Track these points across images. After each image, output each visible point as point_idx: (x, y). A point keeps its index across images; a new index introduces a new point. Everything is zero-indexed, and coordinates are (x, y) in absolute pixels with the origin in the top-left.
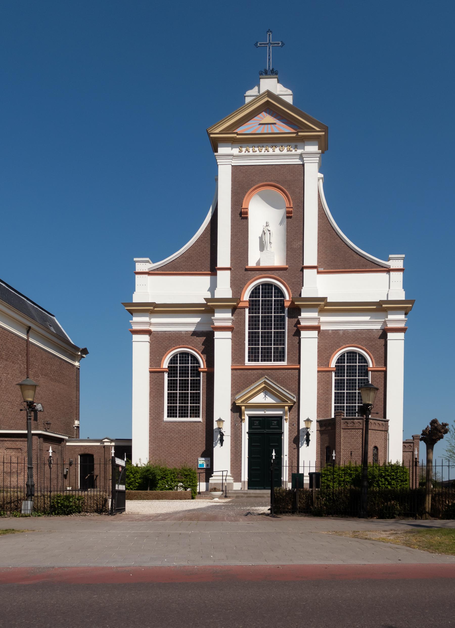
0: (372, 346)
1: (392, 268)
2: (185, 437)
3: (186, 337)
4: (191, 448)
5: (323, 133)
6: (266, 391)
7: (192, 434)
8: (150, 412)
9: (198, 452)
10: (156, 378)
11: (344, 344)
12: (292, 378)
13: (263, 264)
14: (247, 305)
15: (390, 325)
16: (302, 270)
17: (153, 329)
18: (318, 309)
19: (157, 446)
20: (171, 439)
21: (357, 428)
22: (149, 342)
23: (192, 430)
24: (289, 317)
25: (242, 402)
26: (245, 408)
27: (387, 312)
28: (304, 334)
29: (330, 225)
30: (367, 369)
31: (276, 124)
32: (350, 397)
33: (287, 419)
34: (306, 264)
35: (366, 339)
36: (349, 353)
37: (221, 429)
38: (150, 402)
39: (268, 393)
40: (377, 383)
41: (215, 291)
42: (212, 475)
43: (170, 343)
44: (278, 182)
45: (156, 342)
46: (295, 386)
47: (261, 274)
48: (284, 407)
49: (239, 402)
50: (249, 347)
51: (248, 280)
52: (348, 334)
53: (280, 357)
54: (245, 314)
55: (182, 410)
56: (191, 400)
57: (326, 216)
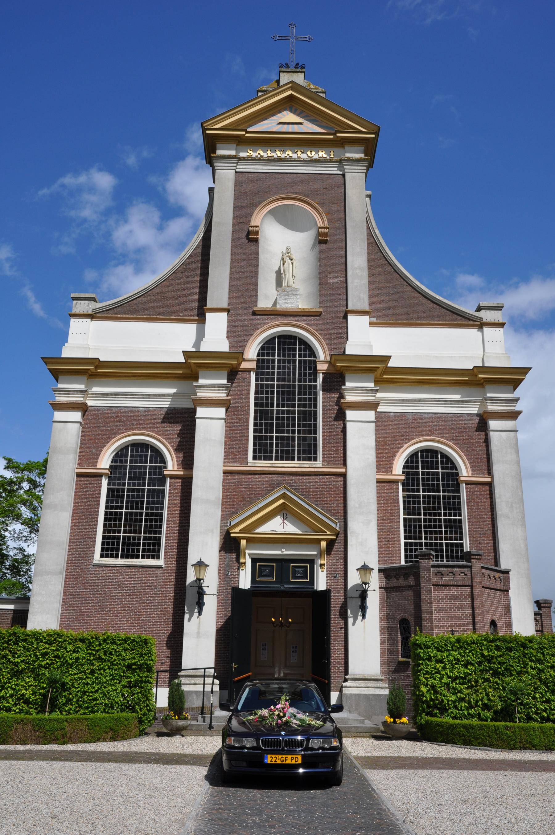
0: (463, 441)
1: (484, 321)
2: (130, 595)
3: (145, 417)
4: (139, 618)
5: (373, 136)
6: (284, 512)
7: (144, 590)
8: (69, 546)
9: (153, 625)
10: (87, 486)
11: (416, 435)
12: (331, 489)
13: (282, 306)
14: (253, 365)
15: (491, 407)
16: (345, 318)
17: (90, 402)
18: (372, 376)
19: (77, 612)
20: (104, 598)
21: (460, 583)
22: (80, 423)
23: (145, 583)
24: (324, 390)
25: (241, 531)
26: (247, 542)
27: (483, 387)
28: (350, 415)
29: (383, 257)
30: (457, 480)
31: (302, 124)
32: (430, 527)
33: (324, 565)
34: (351, 307)
35: (452, 429)
36: (425, 451)
37: (202, 581)
38: (72, 528)
39: (289, 516)
40: (478, 503)
41: (202, 342)
42: (179, 674)
43: (117, 427)
44: (305, 195)
45: (94, 424)
46: (337, 504)
47: (278, 320)
48: (318, 541)
49: (237, 530)
50: (254, 436)
51: (257, 328)
52: (422, 420)
53: (310, 452)
54: (250, 380)
55: (129, 544)
56: (146, 526)
57: (378, 245)
